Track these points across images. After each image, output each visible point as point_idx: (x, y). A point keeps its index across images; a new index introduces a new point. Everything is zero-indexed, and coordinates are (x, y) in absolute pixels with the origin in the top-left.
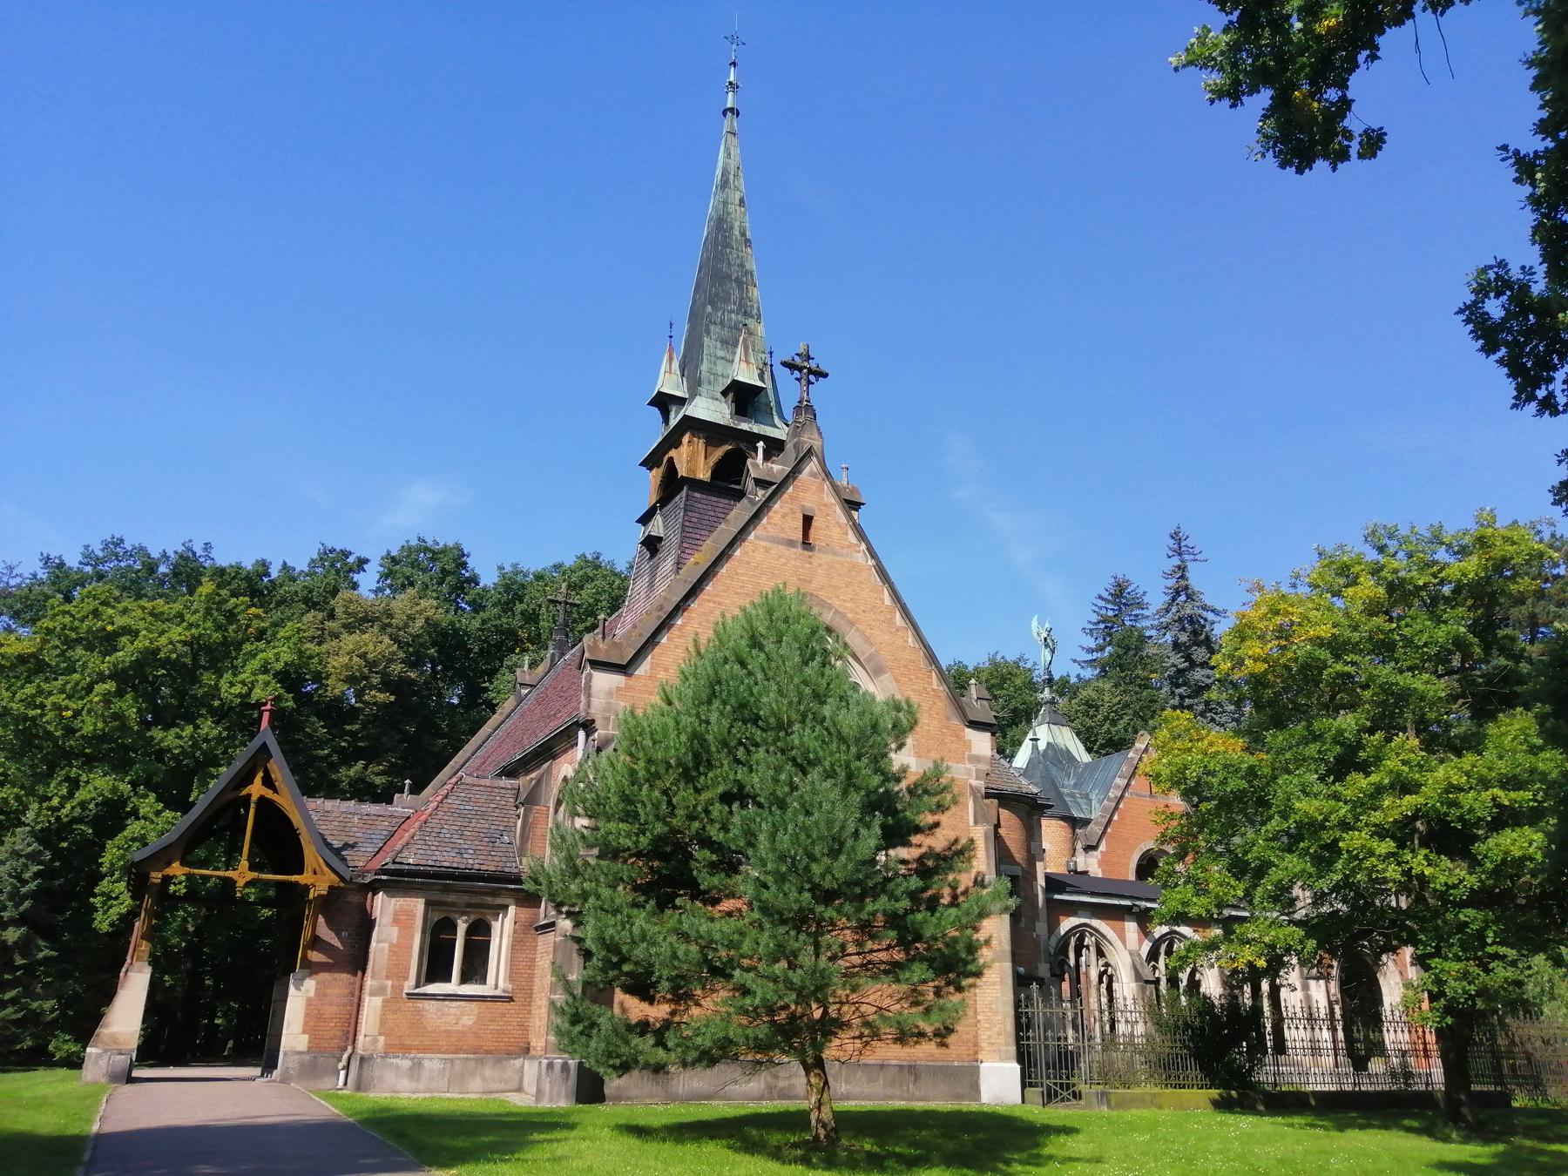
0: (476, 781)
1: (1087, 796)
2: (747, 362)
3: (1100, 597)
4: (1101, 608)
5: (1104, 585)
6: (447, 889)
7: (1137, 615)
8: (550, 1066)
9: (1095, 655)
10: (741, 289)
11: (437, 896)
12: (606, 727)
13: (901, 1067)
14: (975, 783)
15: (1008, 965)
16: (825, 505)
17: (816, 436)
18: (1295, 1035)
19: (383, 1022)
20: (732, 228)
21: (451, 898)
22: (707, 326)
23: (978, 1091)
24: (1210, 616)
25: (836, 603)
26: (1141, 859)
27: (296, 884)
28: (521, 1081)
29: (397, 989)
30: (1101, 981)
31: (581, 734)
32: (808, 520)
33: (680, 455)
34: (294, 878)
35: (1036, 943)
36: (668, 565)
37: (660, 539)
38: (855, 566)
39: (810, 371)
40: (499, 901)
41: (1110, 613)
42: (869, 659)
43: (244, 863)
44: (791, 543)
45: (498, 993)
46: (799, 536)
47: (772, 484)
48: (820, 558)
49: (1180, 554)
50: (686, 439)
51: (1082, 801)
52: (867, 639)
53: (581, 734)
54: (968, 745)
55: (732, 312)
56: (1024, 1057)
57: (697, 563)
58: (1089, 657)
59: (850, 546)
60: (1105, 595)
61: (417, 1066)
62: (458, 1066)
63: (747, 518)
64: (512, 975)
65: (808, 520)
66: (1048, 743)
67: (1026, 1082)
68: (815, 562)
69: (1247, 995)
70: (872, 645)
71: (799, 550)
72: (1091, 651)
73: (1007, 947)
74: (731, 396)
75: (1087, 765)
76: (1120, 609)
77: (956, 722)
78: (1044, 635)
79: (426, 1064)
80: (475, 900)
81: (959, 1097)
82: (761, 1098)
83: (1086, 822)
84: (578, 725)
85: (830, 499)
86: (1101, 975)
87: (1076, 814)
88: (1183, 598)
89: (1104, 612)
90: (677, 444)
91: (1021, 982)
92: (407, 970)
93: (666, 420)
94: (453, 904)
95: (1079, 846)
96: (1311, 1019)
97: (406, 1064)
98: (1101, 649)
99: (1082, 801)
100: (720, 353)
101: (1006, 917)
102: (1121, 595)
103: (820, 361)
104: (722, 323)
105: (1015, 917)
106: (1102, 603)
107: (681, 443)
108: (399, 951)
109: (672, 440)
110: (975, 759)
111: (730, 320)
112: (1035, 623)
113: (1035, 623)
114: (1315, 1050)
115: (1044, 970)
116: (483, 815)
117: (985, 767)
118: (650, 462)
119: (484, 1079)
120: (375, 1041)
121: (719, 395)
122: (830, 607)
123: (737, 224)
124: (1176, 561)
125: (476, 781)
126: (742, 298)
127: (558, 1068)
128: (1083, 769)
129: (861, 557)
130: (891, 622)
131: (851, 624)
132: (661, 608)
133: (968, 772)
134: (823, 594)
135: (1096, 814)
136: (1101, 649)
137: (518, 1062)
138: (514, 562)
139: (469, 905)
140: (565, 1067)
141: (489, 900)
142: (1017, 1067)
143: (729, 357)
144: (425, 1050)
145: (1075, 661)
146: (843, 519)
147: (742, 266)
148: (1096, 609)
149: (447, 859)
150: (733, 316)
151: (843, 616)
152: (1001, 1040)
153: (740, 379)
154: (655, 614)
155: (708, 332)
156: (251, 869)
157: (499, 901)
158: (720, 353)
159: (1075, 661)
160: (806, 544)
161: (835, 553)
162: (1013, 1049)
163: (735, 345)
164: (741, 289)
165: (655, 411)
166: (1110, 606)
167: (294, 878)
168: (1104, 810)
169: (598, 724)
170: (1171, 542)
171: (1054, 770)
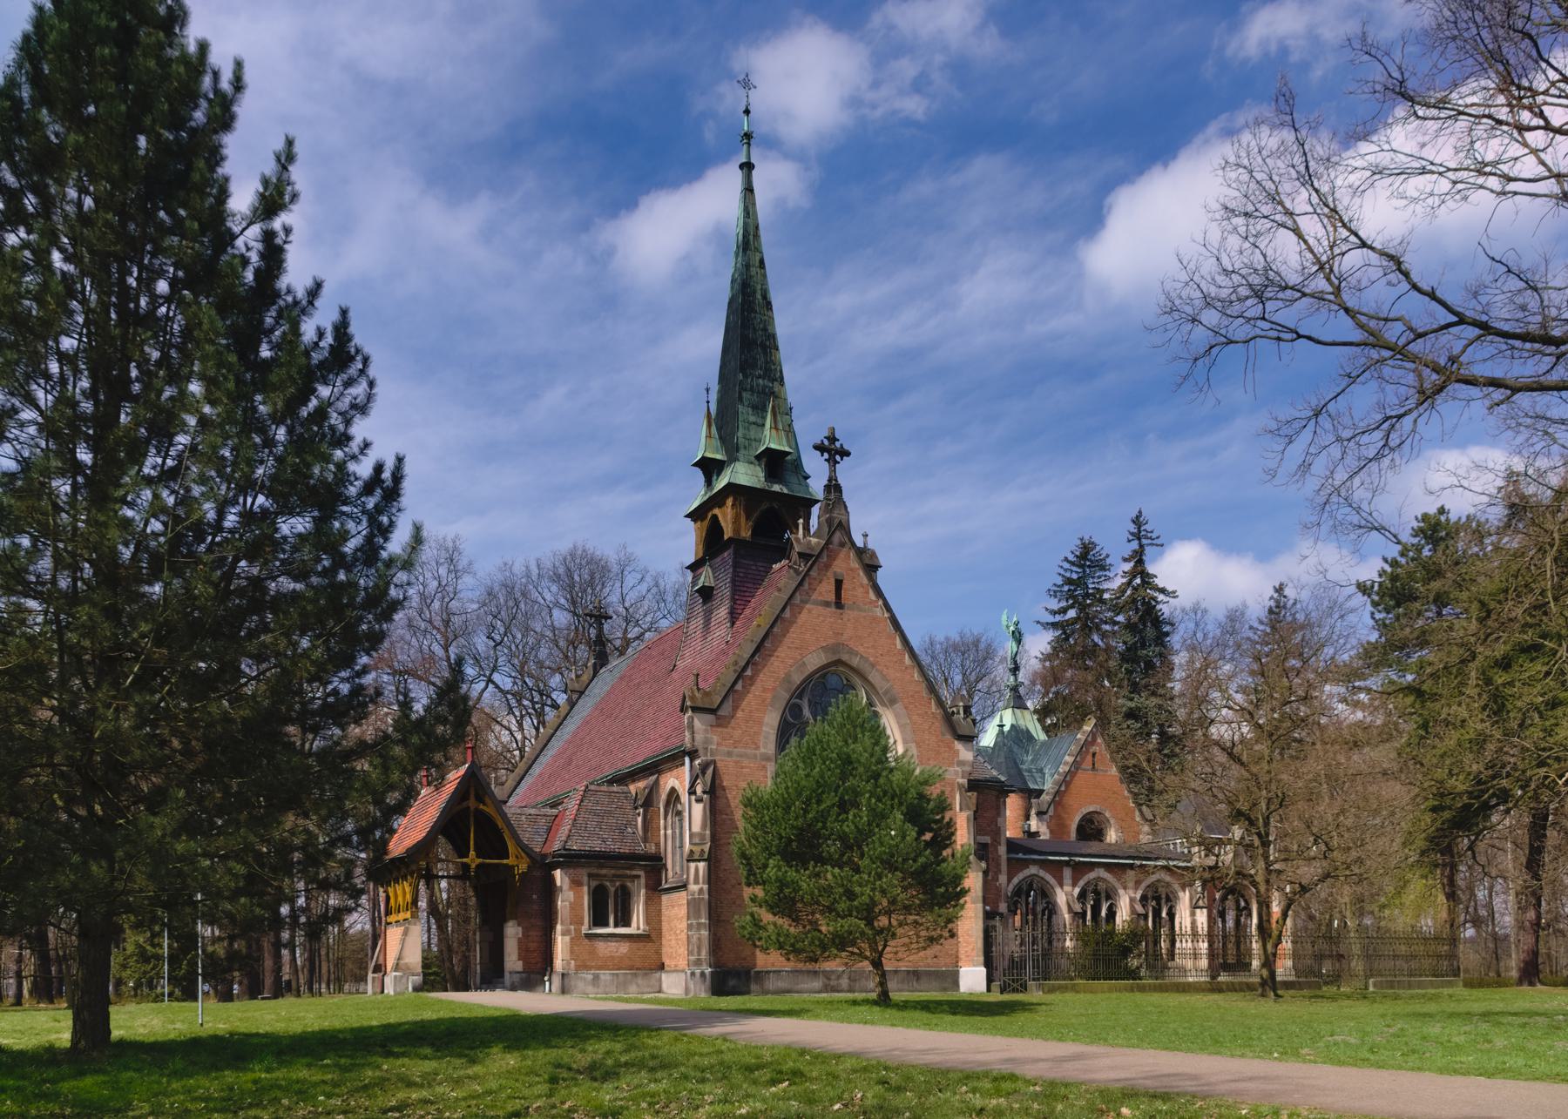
0: (598, 788)
1: (1041, 771)
2: (776, 429)
3: (1066, 559)
4: (1066, 570)
5: (1070, 548)
6: (601, 866)
7: (1099, 577)
8: (693, 974)
9: (1058, 618)
10: (765, 353)
11: (595, 871)
12: (706, 755)
13: (908, 972)
14: (961, 780)
15: (980, 905)
16: (852, 570)
17: (843, 511)
18: (1183, 945)
19: (572, 952)
20: (755, 292)
21: (604, 871)
22: (740, 393)
23: (958, 986)
24: (1161, 597)
25: (861, 650)
26: (1082, 820)
27: (506, 865)
28: (660, 986)
29: (578, 931)
30: (1043, 914)
31: (687, 760)
32: (839, 584)
33: (725, 516)
34: (505, 861)
35: (998, 889)
36: (722, 612)
37: (712, 589)
38: (875, 619)
39: (837, 452)
40: (634, 873)
41: (1075, 576)
42: (886, 693)
43: (472, 853)
44: (827, 604)
45: (640, 932)
46: (832, 597)
47: (812, 556)
48: (849, 614)
49: (1139, 539)
50: (729, 502)
51: (1037, 776)
52: (884, 677)
53: (687, 760)
54: (957, 753)
55: (759, 377)
56: (988, 963)
57: (759, 626)
58: (1051, 619)
59: (871, 602)
60: (1071, 558)
61: (596, 978)
62: (621, 978)
63: (794, 586)
64: (648, 921)
65: (839, 584)
66: (1012, 726)
67: (990, 980)
68: (845, 617)
69: (1254, 926)
70: (888, 681)
71: (833, 609)
72: (1054, 613)
73: (980, 894)
74: (764, 460)
75: (1044, 743)
76: (1084, 572)
77: (949, 737)
78: (1012, 628)
79: (602, 977)
80: (620, 872)
81: (945, 989)
82: (819, 992)
83: (1040, 792)
84: (684, 753)
85: (855, 564)
86: (1043, 911)
87: (1032, 786)
88: (1138, 581)
89: (1068, 575)
90: (721, 505)
91: (989, 916)
92: (583, 918)
93: (709, 483)
94: (605, 876)
95: (1033, 812)
96: (1195, 934)
97: (590, 977)
98: (1064, 611)
99: (1037, 776)
100: (752, 419)
101: (981, 874)
102: (1087, 559)
103: (844, 441)
104: (752, 390)
105: (985, 873)
106: (1067, 565)
107: (724, 504)
108: (575, 907)
109: (716, 500)
110: (961, 763)
111: (758, 385)
112: (1004, 617)
113: (1004, 617)
114: (1196, 956)
115: (1003, 907)
116: (610, 812)
117: (968, 769)
118: (695, 516)
119: (638, 986)
120: (569, 964)
121: (753, 459)
122: (857, 654)
123: (759, 287)
124: (1135, 545)
125: (598, 788)
126: (767, 362)
127: (698, 975)
128: (1041, 747)
129: (879, 612)
130: (902, 661)
131: (873, 666)
132: (736, 663)
133: (956, 773)
134: (851, 644)
135: (1049, 785)
136: (1064, 611)
137: (657, 975)
138: (369, 439)
139: (614, 876)
140: (703, 974)
141: (628, 872)
142: (984, 970)
143: (760, 421)
144: (600, 968)
145: (1038, 622)
146: (865, 581)
147: (765, 330)
148: (1062, 572)
149: (596, 845)
150: (761, 381)
151: (867, 660)
152: (974, 953)
153: (773, 446)
154: (732, 668)
155: (740, 399)
156: (478, 857)
157: (634, 873)
158: (752, 419)
159: (1038, 622)
160: (839, 604)
161: (859, 609)
162: (982, 959)
163: (764, 409)
164: (765, 353)
165: (699, 475)
166: (1074, 569)
167: (505, 861)
168: (1054, 783)
169: (701, 752)
170: (1133, 529)
171: (1015, 749)
